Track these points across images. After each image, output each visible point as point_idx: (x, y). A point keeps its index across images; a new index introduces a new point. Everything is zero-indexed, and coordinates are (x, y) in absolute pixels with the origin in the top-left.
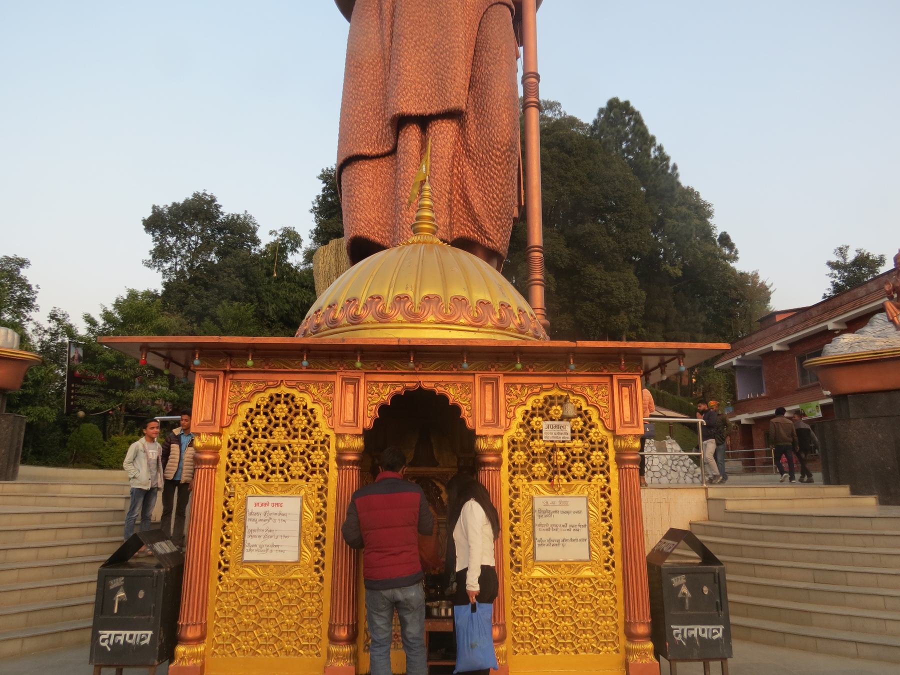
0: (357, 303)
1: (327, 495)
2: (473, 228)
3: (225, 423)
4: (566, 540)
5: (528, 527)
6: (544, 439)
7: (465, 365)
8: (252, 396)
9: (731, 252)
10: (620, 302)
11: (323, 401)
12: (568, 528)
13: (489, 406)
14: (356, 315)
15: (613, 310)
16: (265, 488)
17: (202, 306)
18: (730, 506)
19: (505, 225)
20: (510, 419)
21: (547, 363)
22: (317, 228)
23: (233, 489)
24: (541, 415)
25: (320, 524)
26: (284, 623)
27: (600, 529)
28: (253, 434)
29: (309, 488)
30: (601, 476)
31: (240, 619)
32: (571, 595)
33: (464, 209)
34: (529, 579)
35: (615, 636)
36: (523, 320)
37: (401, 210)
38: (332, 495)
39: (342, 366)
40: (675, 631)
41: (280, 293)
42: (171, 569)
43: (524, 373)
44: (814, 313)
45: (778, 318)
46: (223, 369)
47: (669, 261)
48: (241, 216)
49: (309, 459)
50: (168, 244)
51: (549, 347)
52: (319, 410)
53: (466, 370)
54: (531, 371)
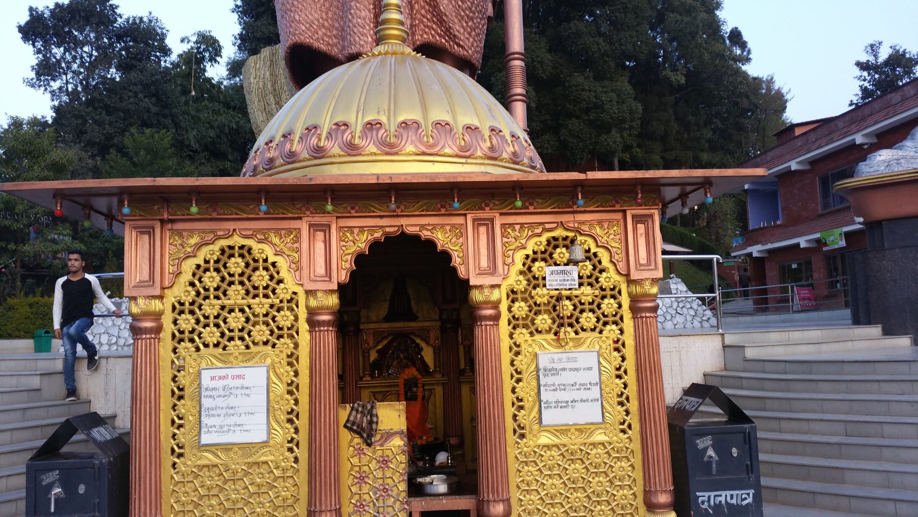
0: (318, 132)
1: (298, 363)
2: (439, 31)
3: (167, 284)
4: (576, 401)
5: (532, 387)
6: (548, 287)
7: (456, 205)
8: (198, 249)
9: (743, 52)
10: (612, 118)
11: (287, 253)
12: (578, 387)
13: (484, 251)
14: (318, 147)
15: (603, 128)
16: (223, 359)
17: (104, 135)
18: (750, 353)
19: (478, 27)
20: (509, 265)
21: (549, 199)
22: (242, 33)
23: (182, 362)
24: (544, 260)
25: (291, 396)
26: (254, 512)
27: (614, 386)
28: (203, 294)
29: (277, 355)
30: (614, 327)
31: (202, 511)
32: (583, 463)
33: (427, 7)
34: (535, 447)
35: (634, 507)
36: (517, 148)
37: (350, 9)
38: (304, 362)
39: (308, 209)
40: (700, 499)
41: (201, 116)
42: (114, 458)
43: (523, 211)
44: (840, 124)
45: (798, 131)
46: (159, 217)
47: (670, 66)
48: (145, 19)
49: (274, 321)
50: (55, 57)
51: (555, 180)
52: (282, 263)
53: (456, 210)
54: (531, 209)
